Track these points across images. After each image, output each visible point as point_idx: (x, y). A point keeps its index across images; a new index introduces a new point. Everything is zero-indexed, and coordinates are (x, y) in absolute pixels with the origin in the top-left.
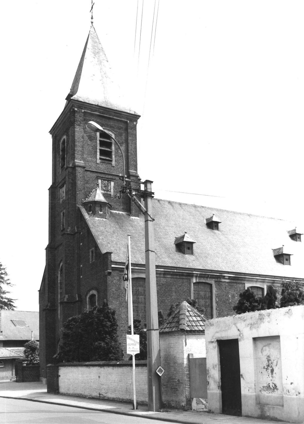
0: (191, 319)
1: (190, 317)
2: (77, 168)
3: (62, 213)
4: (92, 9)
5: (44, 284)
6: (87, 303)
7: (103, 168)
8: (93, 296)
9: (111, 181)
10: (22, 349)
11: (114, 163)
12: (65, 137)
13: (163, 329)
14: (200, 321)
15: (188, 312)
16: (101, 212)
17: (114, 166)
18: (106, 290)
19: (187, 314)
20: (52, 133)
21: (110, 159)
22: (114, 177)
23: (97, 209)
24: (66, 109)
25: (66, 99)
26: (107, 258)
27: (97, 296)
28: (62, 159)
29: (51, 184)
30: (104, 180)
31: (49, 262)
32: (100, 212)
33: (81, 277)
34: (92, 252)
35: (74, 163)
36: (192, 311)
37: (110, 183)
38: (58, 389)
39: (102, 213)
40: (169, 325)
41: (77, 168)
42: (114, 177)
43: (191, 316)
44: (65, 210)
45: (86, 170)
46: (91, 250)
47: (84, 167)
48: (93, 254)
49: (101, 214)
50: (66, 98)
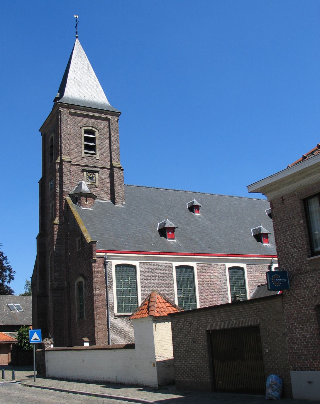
0: (160, 305)
1: (160, 303)
2: (63, 163)
3: (51, 204)
4: (76, 26)
5: (44, 286)
6: (75, 289)
7: (87, 161)
8: (81, 283)
9: (95, 173)
10: (16, 333)
11: (98, 156)
12: (53, 135)
13: (139, 315)
14: (168, 307)
15: (157, 299)
16: (87, 202)
17: (98, 159)
18: (91, 277)
19: (157, 301)
20: (42, 131)
21: (95, 153)
22: (98, 169)
23: (83, 199)
24: (53, 111)
25: (53, 101)
26: (92, 246)
27: (84, 283)
28: (50, 155)
29: (41, 177)
30: (89, 172)
31: (39, 251)
32: (86, 203)
33: (70, 264)
34: (79, 241)
35: (61, 158)
36: (161, 298)
37: (95, 175)
38: (45, 371)
39: (87, 203)
40: (141, 311)
41: (63, 163)
42: (98, 169)
43: (160, 303)
44: (53, 201)
45: (72, 165)
46: (77, 239)
47: (72, 165)
48: (79, 243)
49: (87, 204)
50: (53, 100)
